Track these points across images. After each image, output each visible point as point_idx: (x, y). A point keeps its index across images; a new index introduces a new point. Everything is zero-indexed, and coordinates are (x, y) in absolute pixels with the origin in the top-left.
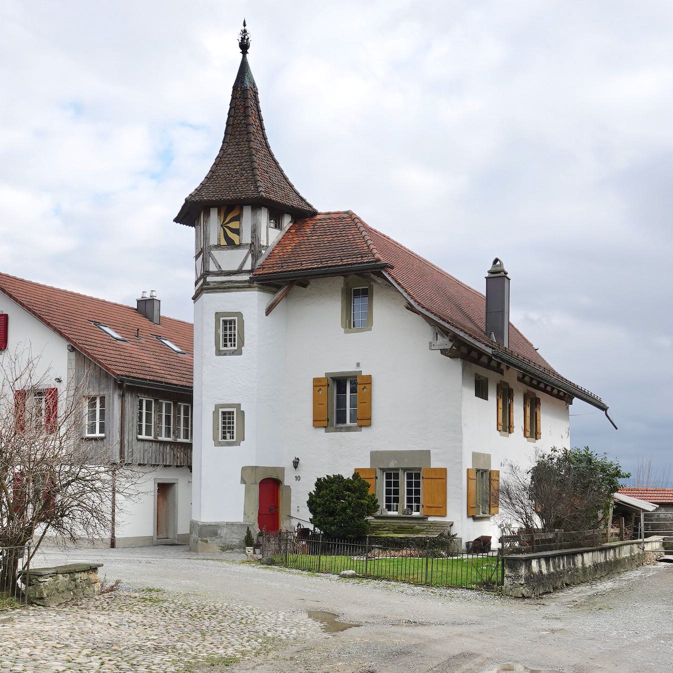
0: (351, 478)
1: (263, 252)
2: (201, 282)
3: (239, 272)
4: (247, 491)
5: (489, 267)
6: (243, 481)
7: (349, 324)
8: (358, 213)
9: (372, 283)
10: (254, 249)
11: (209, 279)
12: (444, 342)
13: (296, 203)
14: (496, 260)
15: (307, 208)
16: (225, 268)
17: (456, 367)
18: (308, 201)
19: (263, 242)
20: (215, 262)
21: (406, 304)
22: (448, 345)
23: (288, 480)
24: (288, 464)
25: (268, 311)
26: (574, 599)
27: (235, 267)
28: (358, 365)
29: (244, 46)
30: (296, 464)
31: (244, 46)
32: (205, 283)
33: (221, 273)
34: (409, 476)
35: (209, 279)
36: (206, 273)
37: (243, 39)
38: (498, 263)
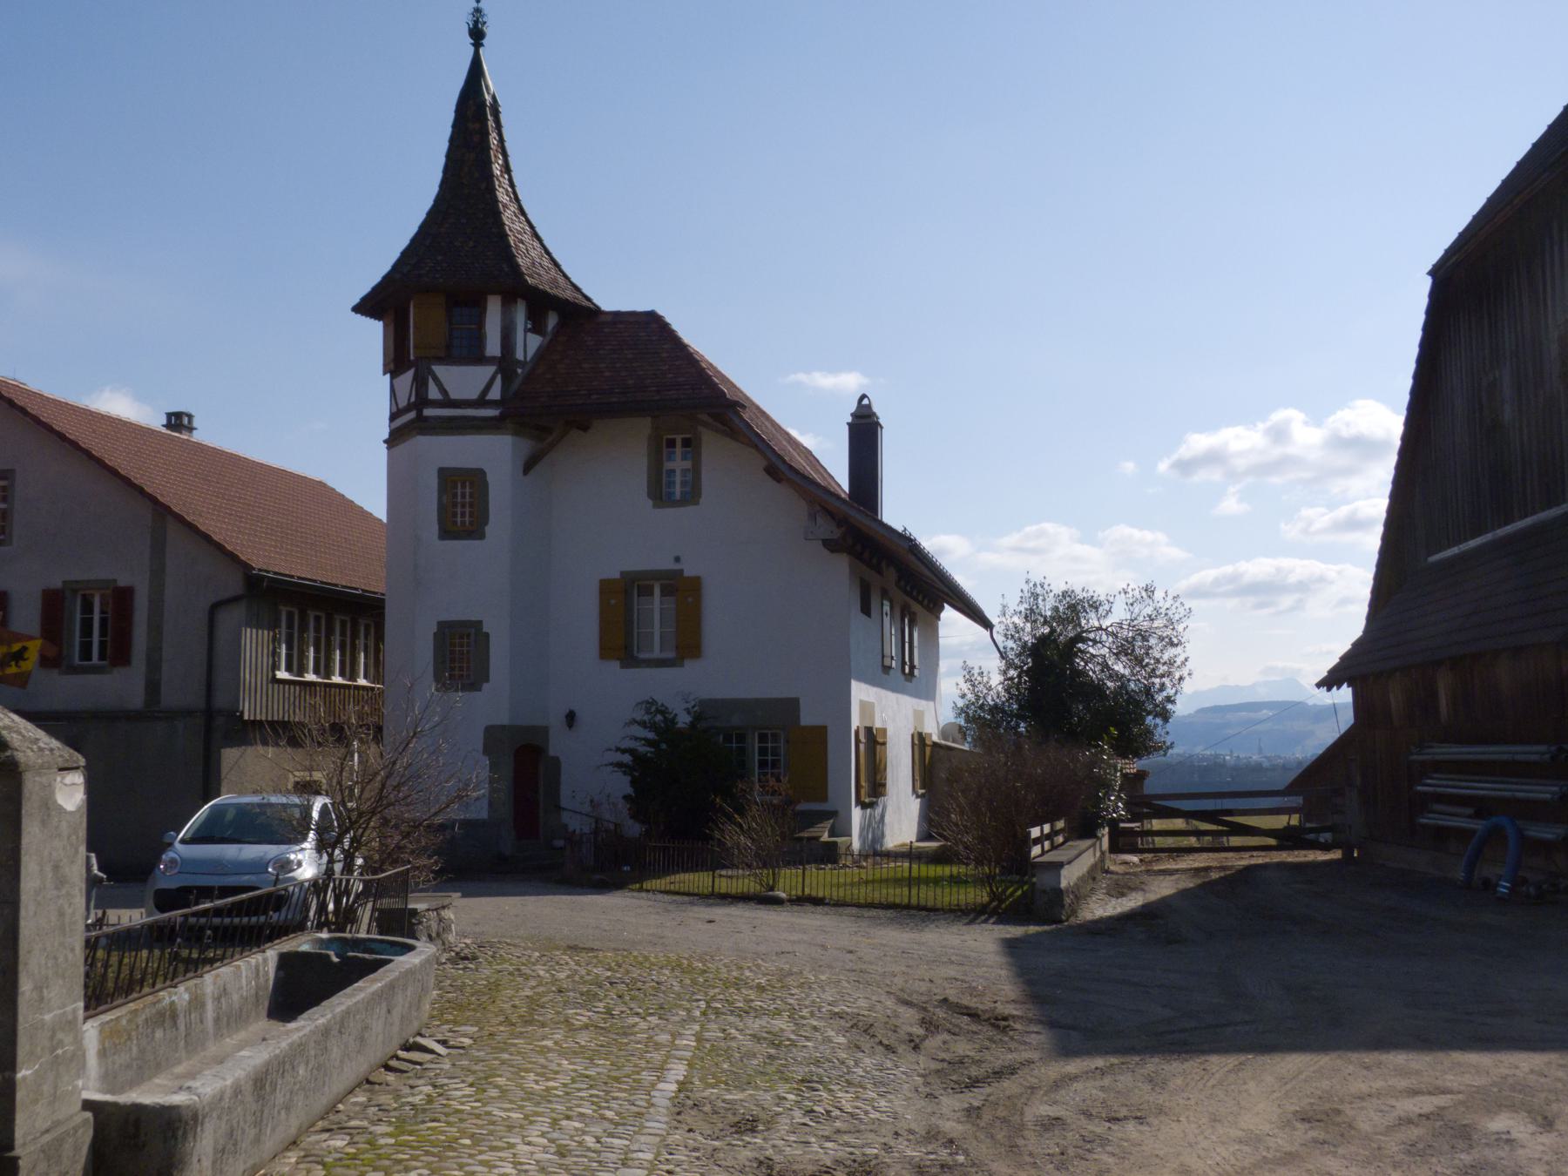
0: (1345, 685)
1: (519, 371)
2: (412, 415)
3: (481, 402)
4: (494, 767)
5: (853, 407)
6: (487, 750)
7: (660, 494)
8: (660, 312)
9: (700, 428)
10: (506, 363)
11: (428, 412)
12: (827, 529)
13: (568, 294)
14: (863, 397)
15: (585, 303)
16: (454, 395)
17: (840, 565)
18: (585, 291)
19: (519, 355)
20: (436, 380)
21: (764, 463)
22: (836, 533)
23: (560, 744)
24: (555, 721)
25: (528, 467)
26: (241, 1170)
27: (474, 394)
28: (677, 559)
29: (477, 35)
30: (571, 718)
31: (477, 35)
32: (420, 418)
33: (449, 403)
34: (763, 738)
35: (428, 412)
36: (421, 401)
37: (476, 22)
38: (865, 402)
